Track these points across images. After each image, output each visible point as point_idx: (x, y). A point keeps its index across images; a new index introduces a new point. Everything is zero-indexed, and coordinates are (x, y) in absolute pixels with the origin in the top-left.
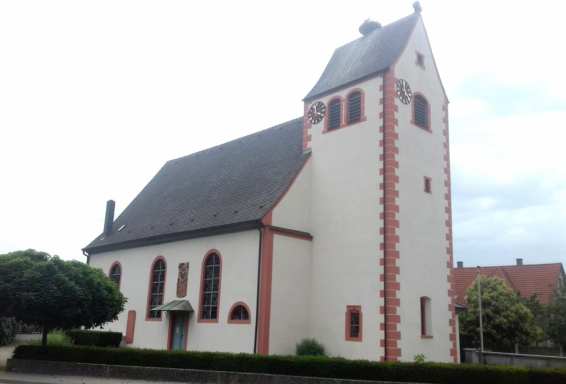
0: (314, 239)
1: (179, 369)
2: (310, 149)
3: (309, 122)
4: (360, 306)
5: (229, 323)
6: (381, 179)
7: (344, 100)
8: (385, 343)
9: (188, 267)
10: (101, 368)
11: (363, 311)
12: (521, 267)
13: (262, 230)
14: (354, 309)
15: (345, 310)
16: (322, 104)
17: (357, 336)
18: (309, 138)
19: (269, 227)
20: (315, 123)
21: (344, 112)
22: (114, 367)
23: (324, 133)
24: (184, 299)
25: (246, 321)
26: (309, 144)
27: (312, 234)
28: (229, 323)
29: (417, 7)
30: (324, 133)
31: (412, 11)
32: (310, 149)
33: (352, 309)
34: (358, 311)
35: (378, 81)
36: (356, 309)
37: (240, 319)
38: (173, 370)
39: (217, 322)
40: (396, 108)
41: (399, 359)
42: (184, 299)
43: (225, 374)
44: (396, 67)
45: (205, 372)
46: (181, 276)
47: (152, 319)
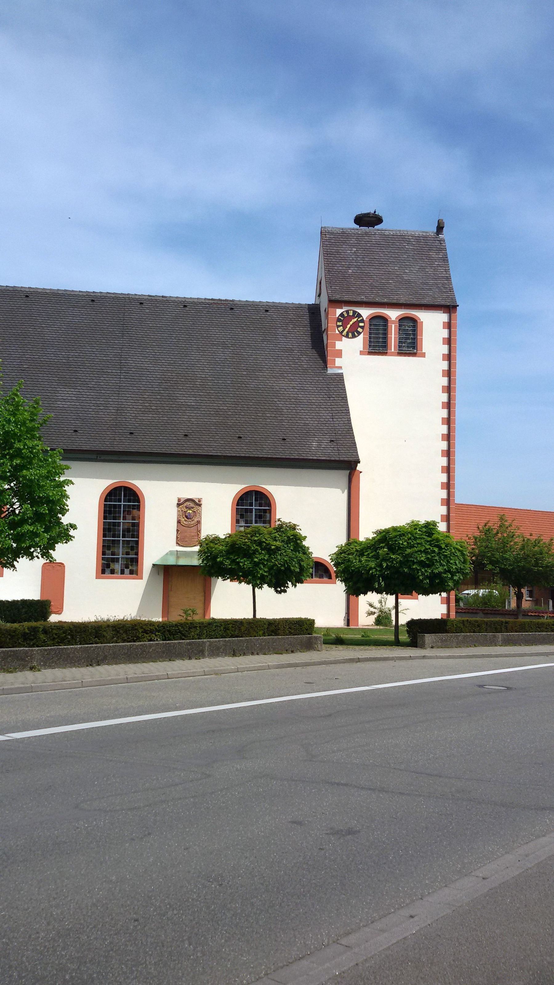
3: (337, 332)
7: (393, 322)
9: (200, 505)
16: (359, 315)
21: (393, 336)
23: (362, 353)
30: (362, 353)
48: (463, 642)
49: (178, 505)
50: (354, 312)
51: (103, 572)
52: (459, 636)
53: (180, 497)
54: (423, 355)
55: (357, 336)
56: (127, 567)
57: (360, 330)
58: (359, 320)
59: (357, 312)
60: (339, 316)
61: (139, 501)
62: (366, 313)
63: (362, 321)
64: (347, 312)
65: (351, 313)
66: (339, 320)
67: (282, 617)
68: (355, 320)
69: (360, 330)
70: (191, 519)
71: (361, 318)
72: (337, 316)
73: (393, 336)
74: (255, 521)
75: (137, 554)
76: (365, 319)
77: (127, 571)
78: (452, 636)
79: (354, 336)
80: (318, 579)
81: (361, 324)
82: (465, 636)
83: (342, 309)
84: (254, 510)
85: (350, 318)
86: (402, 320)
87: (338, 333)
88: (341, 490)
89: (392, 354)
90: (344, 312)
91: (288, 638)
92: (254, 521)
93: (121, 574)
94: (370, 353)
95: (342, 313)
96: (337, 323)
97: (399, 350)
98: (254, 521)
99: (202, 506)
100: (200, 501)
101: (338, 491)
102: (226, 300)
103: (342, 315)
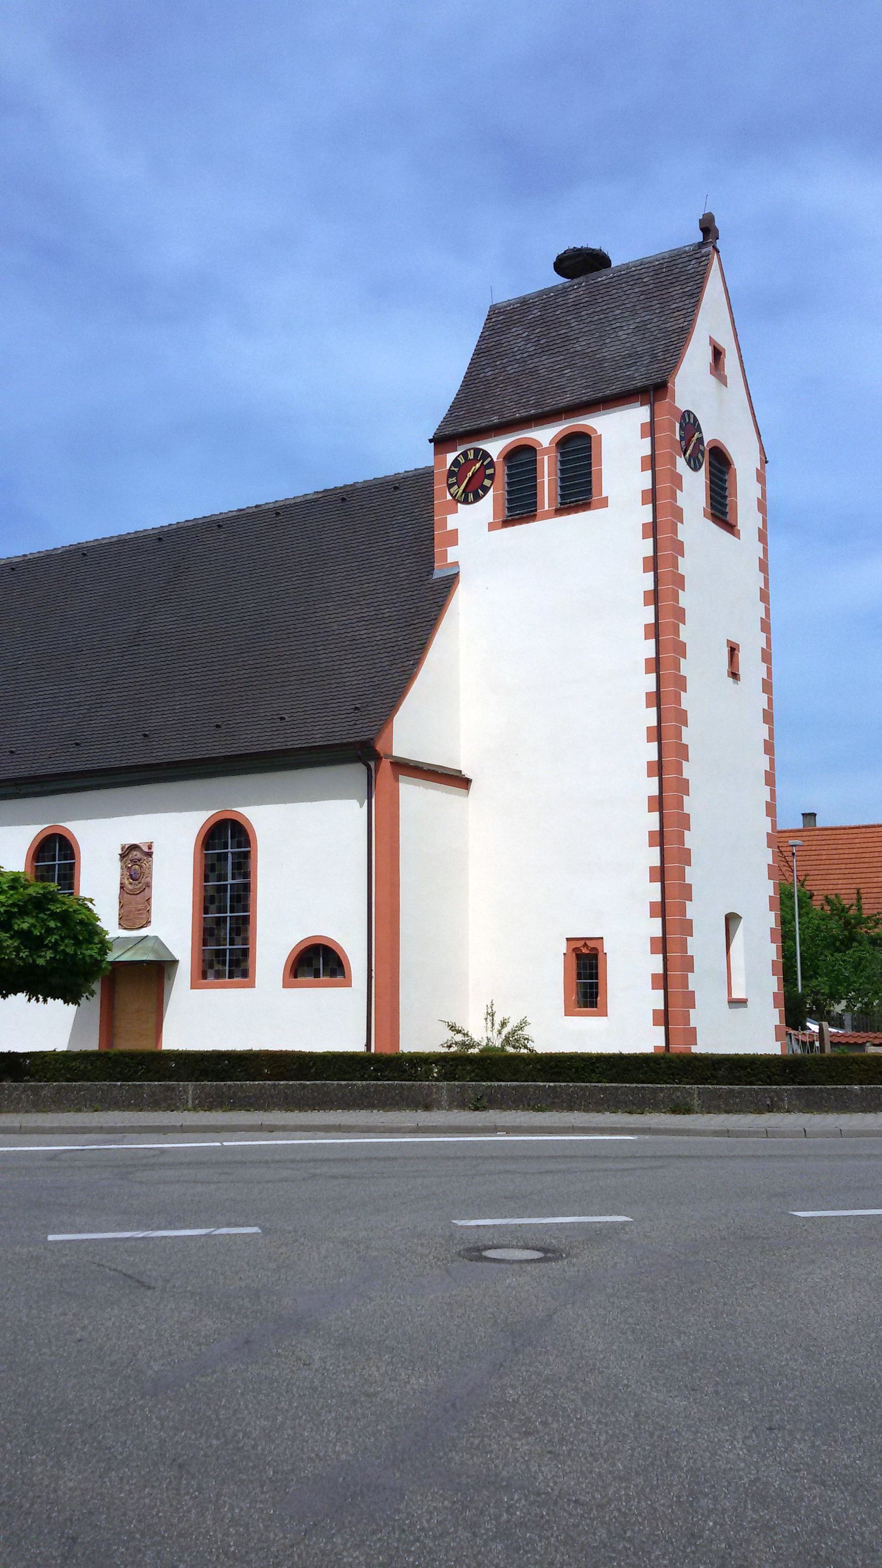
0: (473, 786)
1: (354, 1082)
2: (456, 564)
3: (449, 497)
4: (602, 938)
5: (286, 985)
6: (649, 648)
7: (546, 451)
8: (664, 1018)
9: (150, 855)
10: (172, 1089)
11: (608, 947)
12: (812, 833)
13: (372, 764)
14: (585, 945)
15: (563, 948)
16: (486, 455)
17: (594, 1004)
18: (453, 538)
19: (389, 760)
20: (466, 502)
21: (546, 479)
22: (203, 1087)
23: (492, 527)
24: (143, 932)
25: (339, 978)
26: (453, 554)
27: (467, 773)
28: (286, 985)
29: (708, 228)
30: (492, 527)
31: (699, 237)
32: (456, 564)
33: (580, 944)
34: (595, 949)
35: (639, 414)
36: (591, 944)
37: (317, 975)
38: (341, 1085)
39: (252, 985)
40: (677, 481)
41: (696, 1049)
42: (143, 932)
43: (458, 1086)
44: (678, 380)
45: (413, 1085)
46: (131, 876)
47: (211, 980)
48: (54, 1102)
49: (123, 856)
50: (477, 451)
51: (204, 976)
52: (43, 1087)
53: (124, 843)
54: (604, 503)
55: (483, 496)
56: (211, 966)
57: (487, 482)
58: (485, 463)
59: (481, 449)
60: (451, 467)
61: (72, 856)
62: (495, 447)
63: (492, 464)
64: (465, 454)
65: (471, 456)
66: (451, 473)
67: (284, 1049)
68: (478, 465)
69: (487, 482)
70: (137, 880)
71: (489, 459)
72: (448, 467)
73: (546, 479)
74: (233, 875)
75: (245, 941)
76: (495, 460)
77: (210, 972)
78: (16, 1088)
79: (477, 498)
80: (327, 978)
81: (489, 472)
82: (60, 1088)
83: (456, 451)
84: (230, 855)
85: (469, 463)
86: (564, 442)
87: (451, 498)
88: (358, 801)
89: (547, 516)
90: (458, 456)
91: (80, 1089)
92: (230, 875)
93: (229, 978)
94: (506, 523)
95: (456, 459)
96: (448, 480)
97: (561, 504)
98: (230, 875)
99: (154, 856)
100: (150, 847)
101: (355, 803)
102: (345, 486)
103: (456, 462)
